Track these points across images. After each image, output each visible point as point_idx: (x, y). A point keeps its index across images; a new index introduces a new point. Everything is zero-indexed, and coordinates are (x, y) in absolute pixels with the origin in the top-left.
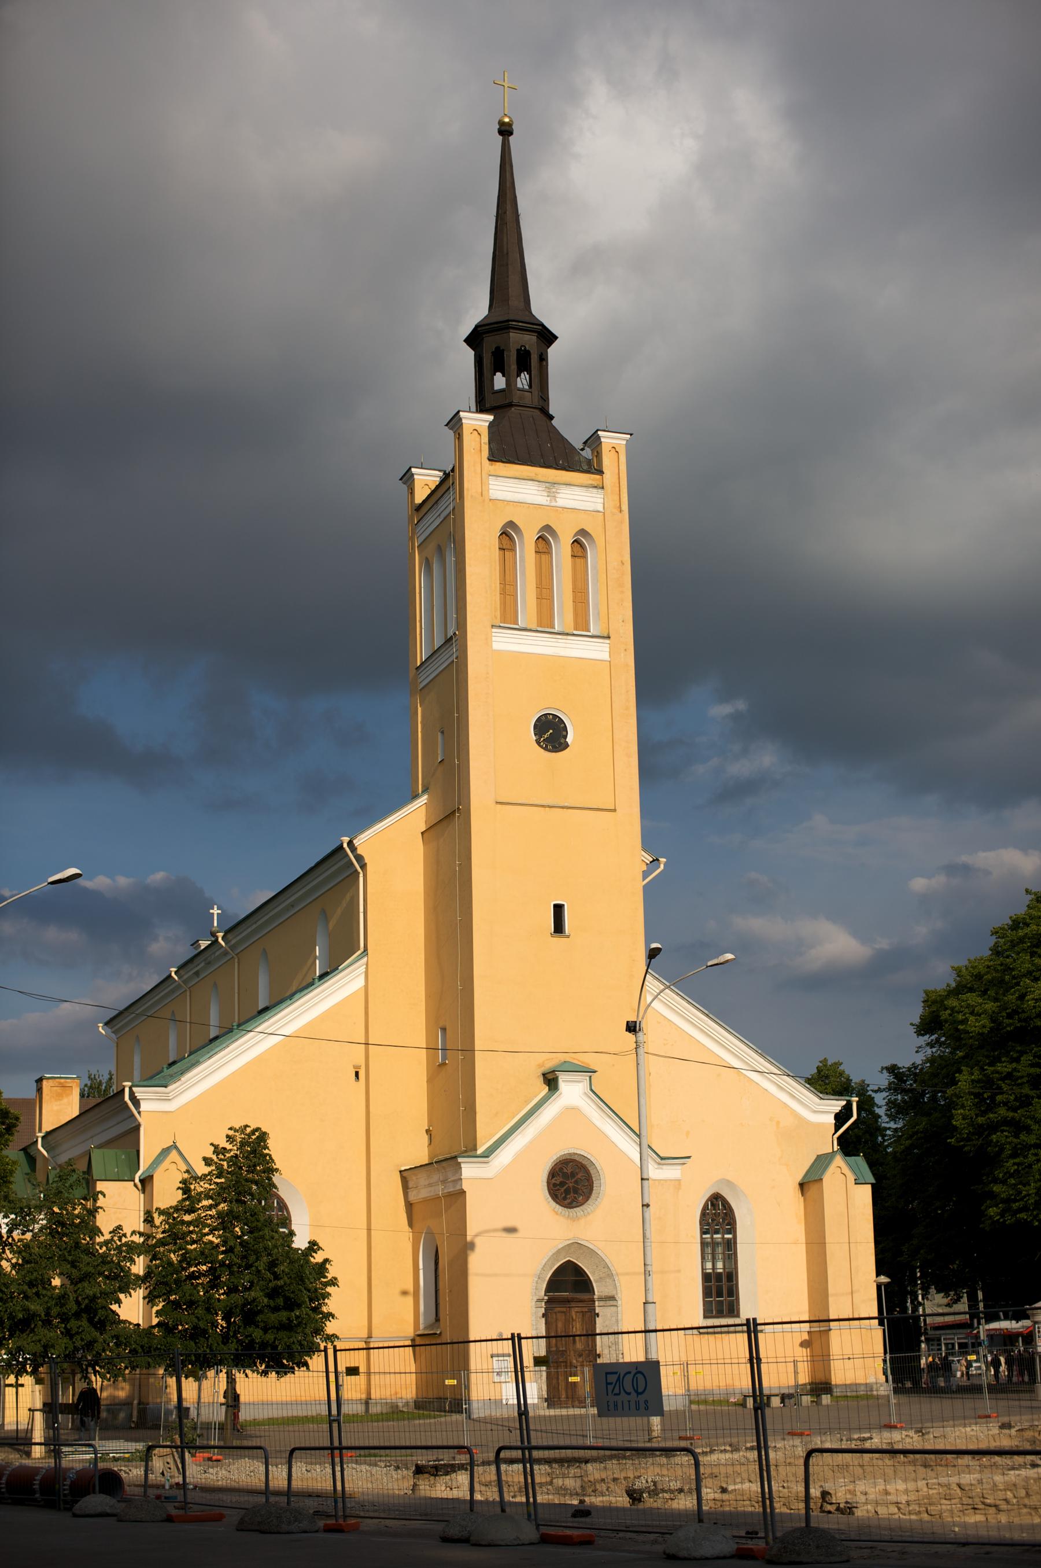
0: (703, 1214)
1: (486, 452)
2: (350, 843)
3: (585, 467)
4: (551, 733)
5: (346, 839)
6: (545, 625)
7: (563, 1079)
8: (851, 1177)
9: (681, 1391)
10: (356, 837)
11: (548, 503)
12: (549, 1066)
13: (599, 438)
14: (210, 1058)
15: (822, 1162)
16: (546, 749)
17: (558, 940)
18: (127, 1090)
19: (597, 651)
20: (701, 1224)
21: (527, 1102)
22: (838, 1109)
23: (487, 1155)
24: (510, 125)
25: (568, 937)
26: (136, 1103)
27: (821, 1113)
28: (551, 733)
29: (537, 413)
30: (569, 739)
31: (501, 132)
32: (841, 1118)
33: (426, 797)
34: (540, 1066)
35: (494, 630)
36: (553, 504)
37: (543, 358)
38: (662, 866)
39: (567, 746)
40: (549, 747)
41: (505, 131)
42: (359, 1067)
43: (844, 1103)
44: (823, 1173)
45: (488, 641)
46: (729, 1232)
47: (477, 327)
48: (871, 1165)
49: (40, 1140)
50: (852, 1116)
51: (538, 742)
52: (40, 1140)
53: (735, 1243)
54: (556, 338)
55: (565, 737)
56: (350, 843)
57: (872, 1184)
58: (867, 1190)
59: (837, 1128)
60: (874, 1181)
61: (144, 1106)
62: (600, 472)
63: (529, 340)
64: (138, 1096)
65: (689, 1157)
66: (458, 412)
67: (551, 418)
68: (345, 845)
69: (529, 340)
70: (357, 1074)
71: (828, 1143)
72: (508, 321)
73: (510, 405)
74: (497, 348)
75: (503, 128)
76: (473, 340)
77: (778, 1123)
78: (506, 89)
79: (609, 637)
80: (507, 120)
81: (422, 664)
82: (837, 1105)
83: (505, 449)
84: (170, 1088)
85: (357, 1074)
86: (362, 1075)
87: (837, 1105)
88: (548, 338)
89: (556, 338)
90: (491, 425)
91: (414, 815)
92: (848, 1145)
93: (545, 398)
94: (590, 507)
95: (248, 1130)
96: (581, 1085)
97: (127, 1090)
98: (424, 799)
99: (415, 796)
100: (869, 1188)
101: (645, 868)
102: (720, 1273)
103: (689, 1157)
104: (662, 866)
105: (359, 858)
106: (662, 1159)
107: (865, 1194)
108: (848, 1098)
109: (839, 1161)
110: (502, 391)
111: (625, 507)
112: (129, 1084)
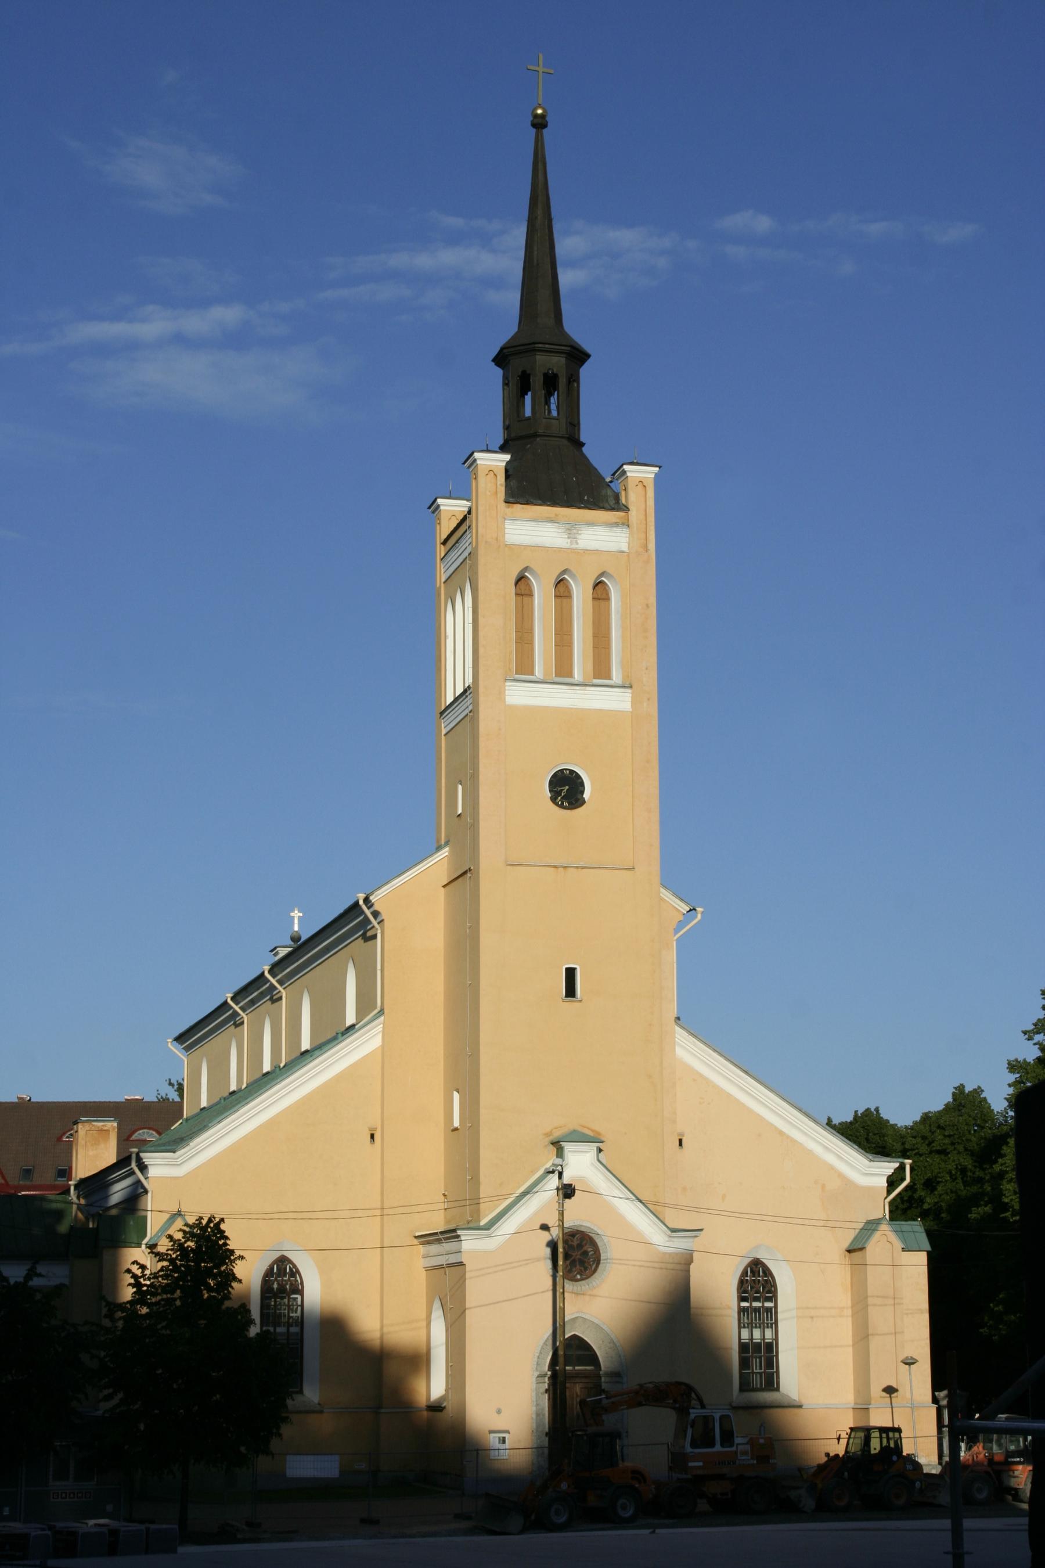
0: (742, 1282)
1: (502, 490)
2: (367, 900)
3: (612, 502)
4: (567, 789)
5: (361, 896)
6: (562, 671)
7: (568, 1147)
8: (898, 1245)
9: (846, 1422)
10: (372, 893)
11: (568, 546)
12: (557, 1135)
13: (624, 472)
14: (219, 1122)
15: (871, 1227)
16: (562, 806)
17: (570, 1006)
18: (134, 1156)
19: (611, 700)
20: (738, 1292)
21: (533, 1172)
22: (890, 1171)
23: (488, 1227)
24: (543, 116)
25: (580, 1001)
26: (143, 1168)
27: (871, 1175)
28: (567, 789)
29: (565, 442)
30: (586, 795)
31: (534, 125)
32: (892, 1182)
33: (447, 849)
34: (547, 1135)
35: (507, 684)
36: (574, 546)
37: (573, 379)
38: (699, 916)
39: (584, 802)
40: (566, 804)
41: (539, 124)
42: (375, 1129)
43: (897, 1165)
44: (865, 1243)
45: (501, 694)
46: (769, 1299)
47: (502, 349)
48: (929, 1234)
49: (72, 1188)
50: (903, 1179)
51: (553, 799)
52: (72, 1188)
53: (776, 1313)
54: (588, 356)
55: (582, 792)
56: (367, 900)
57: (929, 1253)
58: (922, 1258)
59: (889, 1192)
60: (929, 1248)
61: (152, 1172)
62: (626, 509)
63: (557, 363)
64: (147, 1161)
65: (701, 1230)
66: (472, 453)
67: (583, 444)
68: (361, 902)
69: (557, 363)
70: (372, 1136)
71: (880, 1208)
72: (534, 343)
73: (535, 435)
74: (524, 372)
75: (537, 121)
76: (500, 360)
77: (823, 1186)
78: (541, 74)
79: (631, 687)
80: (539, 111)
81: (456, 699)
82: (889, 1167)
83: (526, 487)
84: (178, 1153)
85: (372, 1136)
86: (377, 1137)
87: (889, 1167)
88: (578, 356)
89: (588, 356)
90: (508, 463)
91: (438, 865)
92: (903, 1209)
93: (574, 424)
94: (612, 547)
95: (204, 1222)
96: (588, 1155)
97: (134, 1156)
98: (445, 852)
99: (439, 848)
100: (925, 1254)
101: (681, 918)
102: (759, 1344)
103: (701, 1230)
104: (699, 916)
105: (376, 914)
106: (673, 1230)
107: (919, 1261)
108: (901, 1160)
109: (885, 1227)
110: (529, 419)
111: (652, 546)
112: (135, 1150)
